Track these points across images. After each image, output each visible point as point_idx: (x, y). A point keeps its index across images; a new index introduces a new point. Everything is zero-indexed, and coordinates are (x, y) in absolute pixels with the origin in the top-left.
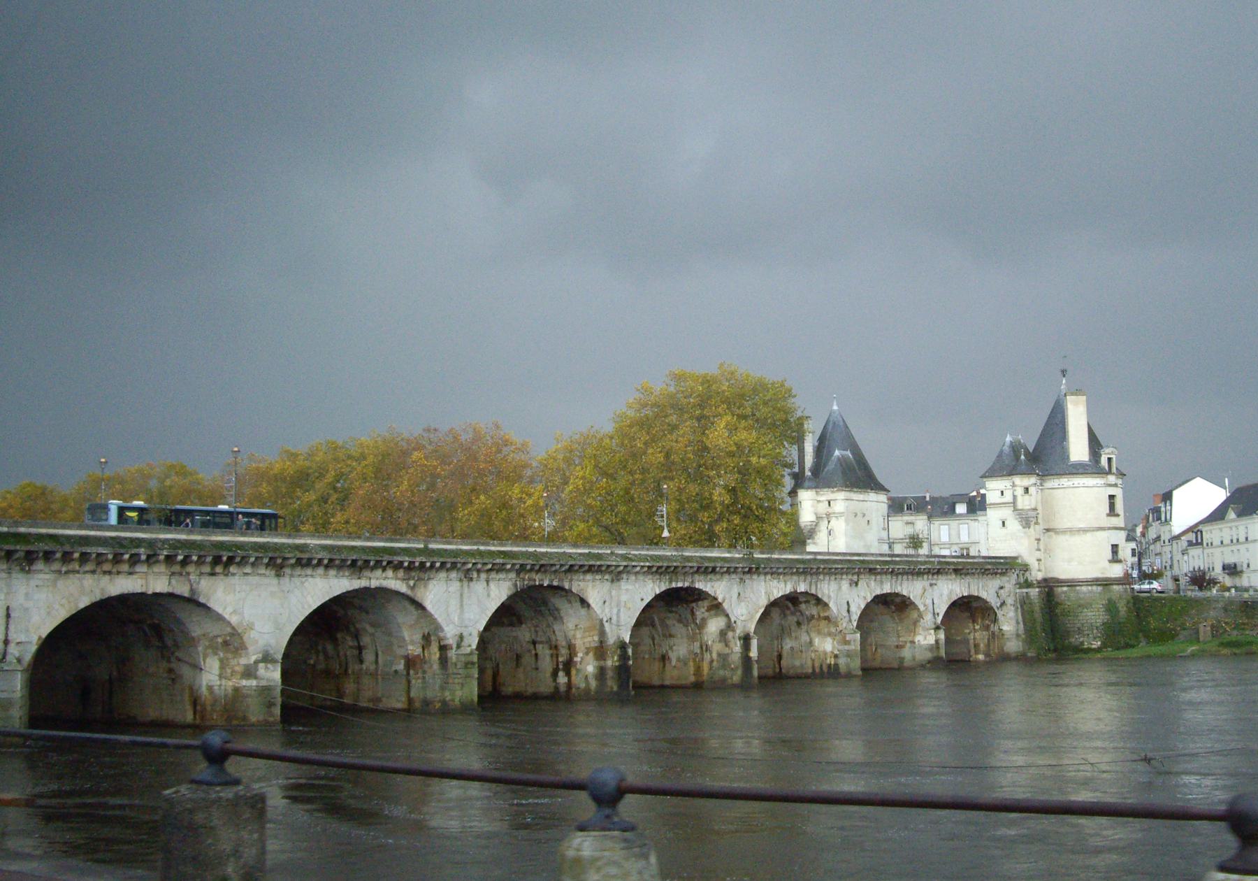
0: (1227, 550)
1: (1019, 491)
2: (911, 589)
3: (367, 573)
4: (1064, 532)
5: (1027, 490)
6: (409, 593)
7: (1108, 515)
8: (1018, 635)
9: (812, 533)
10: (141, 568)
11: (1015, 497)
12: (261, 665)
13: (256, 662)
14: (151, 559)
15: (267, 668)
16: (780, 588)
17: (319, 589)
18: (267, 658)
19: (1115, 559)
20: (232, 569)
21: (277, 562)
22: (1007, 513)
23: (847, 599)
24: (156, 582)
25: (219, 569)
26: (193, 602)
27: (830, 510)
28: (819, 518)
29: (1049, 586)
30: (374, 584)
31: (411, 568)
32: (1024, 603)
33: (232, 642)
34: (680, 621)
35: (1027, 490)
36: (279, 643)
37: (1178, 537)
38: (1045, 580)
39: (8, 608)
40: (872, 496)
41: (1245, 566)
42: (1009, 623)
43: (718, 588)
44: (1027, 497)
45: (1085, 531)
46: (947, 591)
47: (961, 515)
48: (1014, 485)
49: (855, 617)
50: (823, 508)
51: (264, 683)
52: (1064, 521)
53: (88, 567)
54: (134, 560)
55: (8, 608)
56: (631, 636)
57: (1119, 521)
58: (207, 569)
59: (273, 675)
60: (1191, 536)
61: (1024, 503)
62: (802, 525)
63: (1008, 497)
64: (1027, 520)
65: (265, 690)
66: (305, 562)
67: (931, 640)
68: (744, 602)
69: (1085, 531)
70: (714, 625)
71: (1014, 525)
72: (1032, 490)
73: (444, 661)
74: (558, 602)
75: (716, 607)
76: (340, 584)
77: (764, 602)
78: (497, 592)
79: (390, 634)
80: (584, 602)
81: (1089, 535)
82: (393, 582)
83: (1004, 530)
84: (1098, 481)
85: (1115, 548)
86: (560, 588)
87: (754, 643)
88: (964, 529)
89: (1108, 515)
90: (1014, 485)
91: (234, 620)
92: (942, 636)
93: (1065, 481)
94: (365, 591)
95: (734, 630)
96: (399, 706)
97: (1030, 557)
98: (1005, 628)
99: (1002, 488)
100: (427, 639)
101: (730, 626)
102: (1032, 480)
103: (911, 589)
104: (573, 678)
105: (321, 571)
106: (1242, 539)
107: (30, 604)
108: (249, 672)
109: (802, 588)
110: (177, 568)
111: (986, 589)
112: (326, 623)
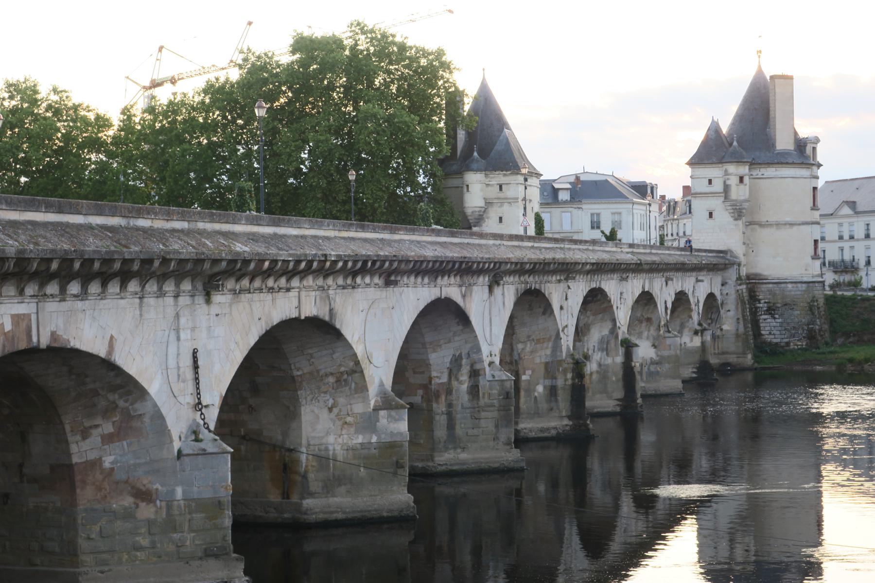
1: (733, 181)
4: (778, 225)
5: (741, 179)
7: (812, 209)
8: (737, 336)
9: (480, 219)
12: (382, 413)
13: (376, 409)
15: (389, 416)
18: (386, 404)
22: (716, 203)
27: (501, 195)
28: (488, 203)
35: (741, 179)
39: (195, 353)
41: (862, 263)
44: (742, 186)
45: (792, 225)
47: (565, 202)
48: (726, 173)
49: (214, 394)
50: (493, 192)
51: (386, 439)
52: (769, 214)
55: (195, 353)
56: (394, 383)
61: (739, 193)
62: (469, 211)
63: (718, 186)
64: (737, 212)
65: (390, 447)
67: (697, 342)
69: (792, 225)
71: (723, 216)
73: (474, 391)
81: (795, 228)
83: (711, 221)
84: (804, 172)
88: (566, 217)
89: (812, 209)
90: (726, 173)
93: (770, 172)
95: (617, 337)
96: (588, 404)
97: (739, 250)
98: (725, 327)
99: (710, 176)
100: (456, 361)
102: (744, 170)
104: (522, 400)
108: (369, 423)
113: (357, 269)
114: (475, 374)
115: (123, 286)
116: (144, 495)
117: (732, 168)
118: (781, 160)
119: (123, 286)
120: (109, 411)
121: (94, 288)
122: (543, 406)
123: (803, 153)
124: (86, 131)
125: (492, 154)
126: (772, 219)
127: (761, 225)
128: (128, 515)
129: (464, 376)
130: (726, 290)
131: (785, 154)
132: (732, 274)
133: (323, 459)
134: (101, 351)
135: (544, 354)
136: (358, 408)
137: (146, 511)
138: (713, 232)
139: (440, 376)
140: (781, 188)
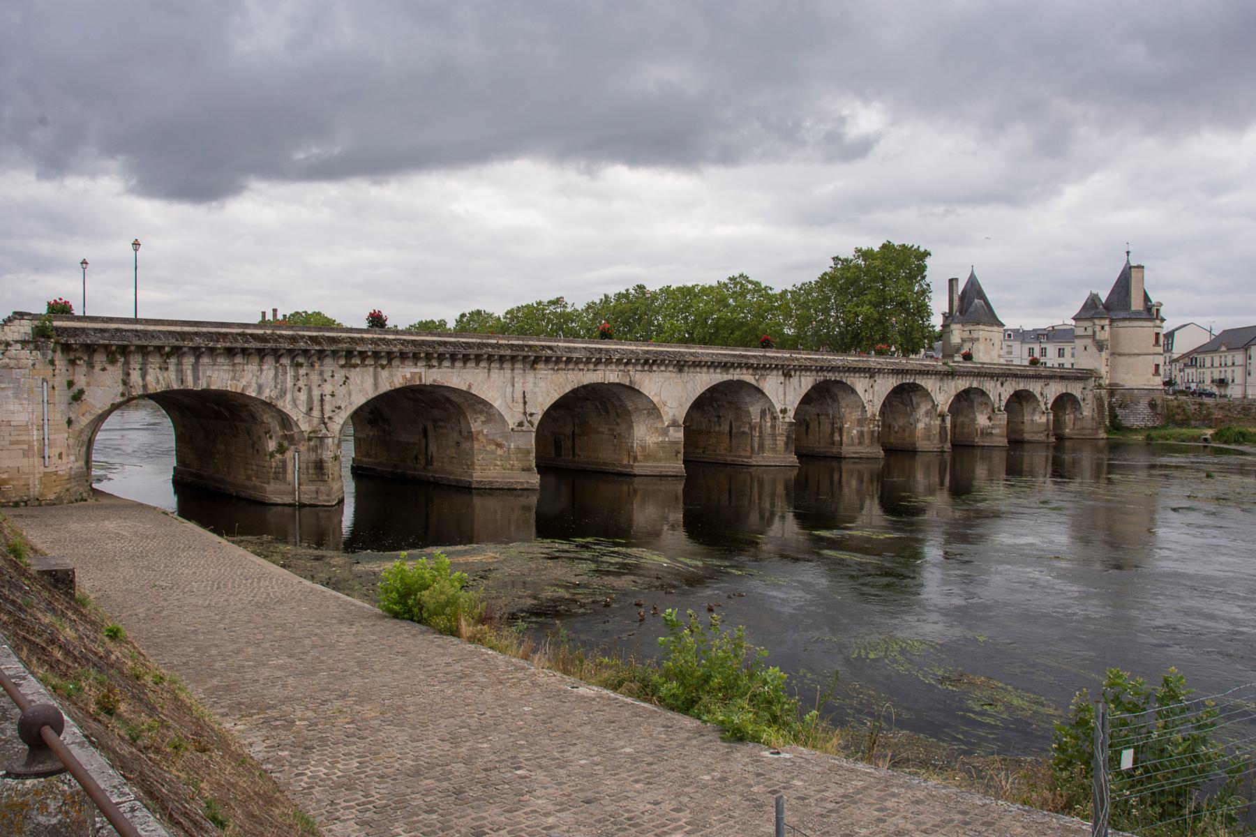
0: (1216, 371)
1: (1098, 328)
2: (1035, 387)
3: (731, 371)
5: (1103, 328)
6: (754, 383)
10: (601, 367)
11: (1094, 332)
14: (609, 362)
16: (962, 384)
17: (704, 381)
18: (674, 424)
19: (1157, 372)
20: (655, 368)
21: (681, 365)
22: (1089, 342)
23: (1000, 392)
24: (611, 376)
25: (646, 368)
26: (632, 390)
28: (963, 340)
29: (1112, 390)
30: (736, 378)
31: (756, 369)
32: (1099, 400)
33: (653, 411)
34: (902, 403)
36: (681, 415)
37: (1177, 360)
38: (1110, 385)
40: (996, 328)
42: (1087, 411)
43: (929, 384)
46: (1054, 390)
49: (1003, 403)
50: (966, 335)
53: (571, 366)
54: (598, 362)
57: (1160, 350)
58: (639, 368)
59: (678, 435)
60: (1187, 360)
63: (1090, 332)
64: (1100, 346)
66: (698, 365)
67: (1044, 419)
68: (942, 394)
70: (924, 408)
71: (1092, 350)
72: (1107, 328)
73: (773, 427)
74: (841, 394)
75: (927, 395)
76: (718, 377)
77: (953, 393)
78: (806, 383)
79: (740, 409)
80: (853, 391)
82: (748, 377)
85: (1157, 366)
86: (841, 382)
87: (948, 419)
91: (655, 400)
92: (1051, 417)
94: (730, 382)
97: (1103, 370)
100: (763, 413)
101: (935, 406)
103: (1035, 387)
105: (705, 369)
106: (1229, 363)
107: (536, 390)
108: (665, 432)
109: (975, 385)
110: (622, 367)
111: (1076, 389)
112: (704, 404)
113: (649, 363)
114: (774, 418)
115: (477, 364)
116: (499, 445)
117: (1097, 322)
118: (1136, 317)
119: (477, 364)
120: (481, 412)
121: (459, 364)
122: (857, 441)
123: (1151, 312)
124: (768, 302)
125: (971, 310)
126: (1127, 351)
127: (1120, 355)
128: (493, 453)
129: (768, 418)
130: (1085, 392)
131: (1137, 312)
132: (1091, 383)
133: (643, 448)
134: (465, 388)
135: (857, 414)
136: (659, 425)
137: (499, 452)
138: (1082, 357)
139: (756, 418)
140: (1138, 335)
